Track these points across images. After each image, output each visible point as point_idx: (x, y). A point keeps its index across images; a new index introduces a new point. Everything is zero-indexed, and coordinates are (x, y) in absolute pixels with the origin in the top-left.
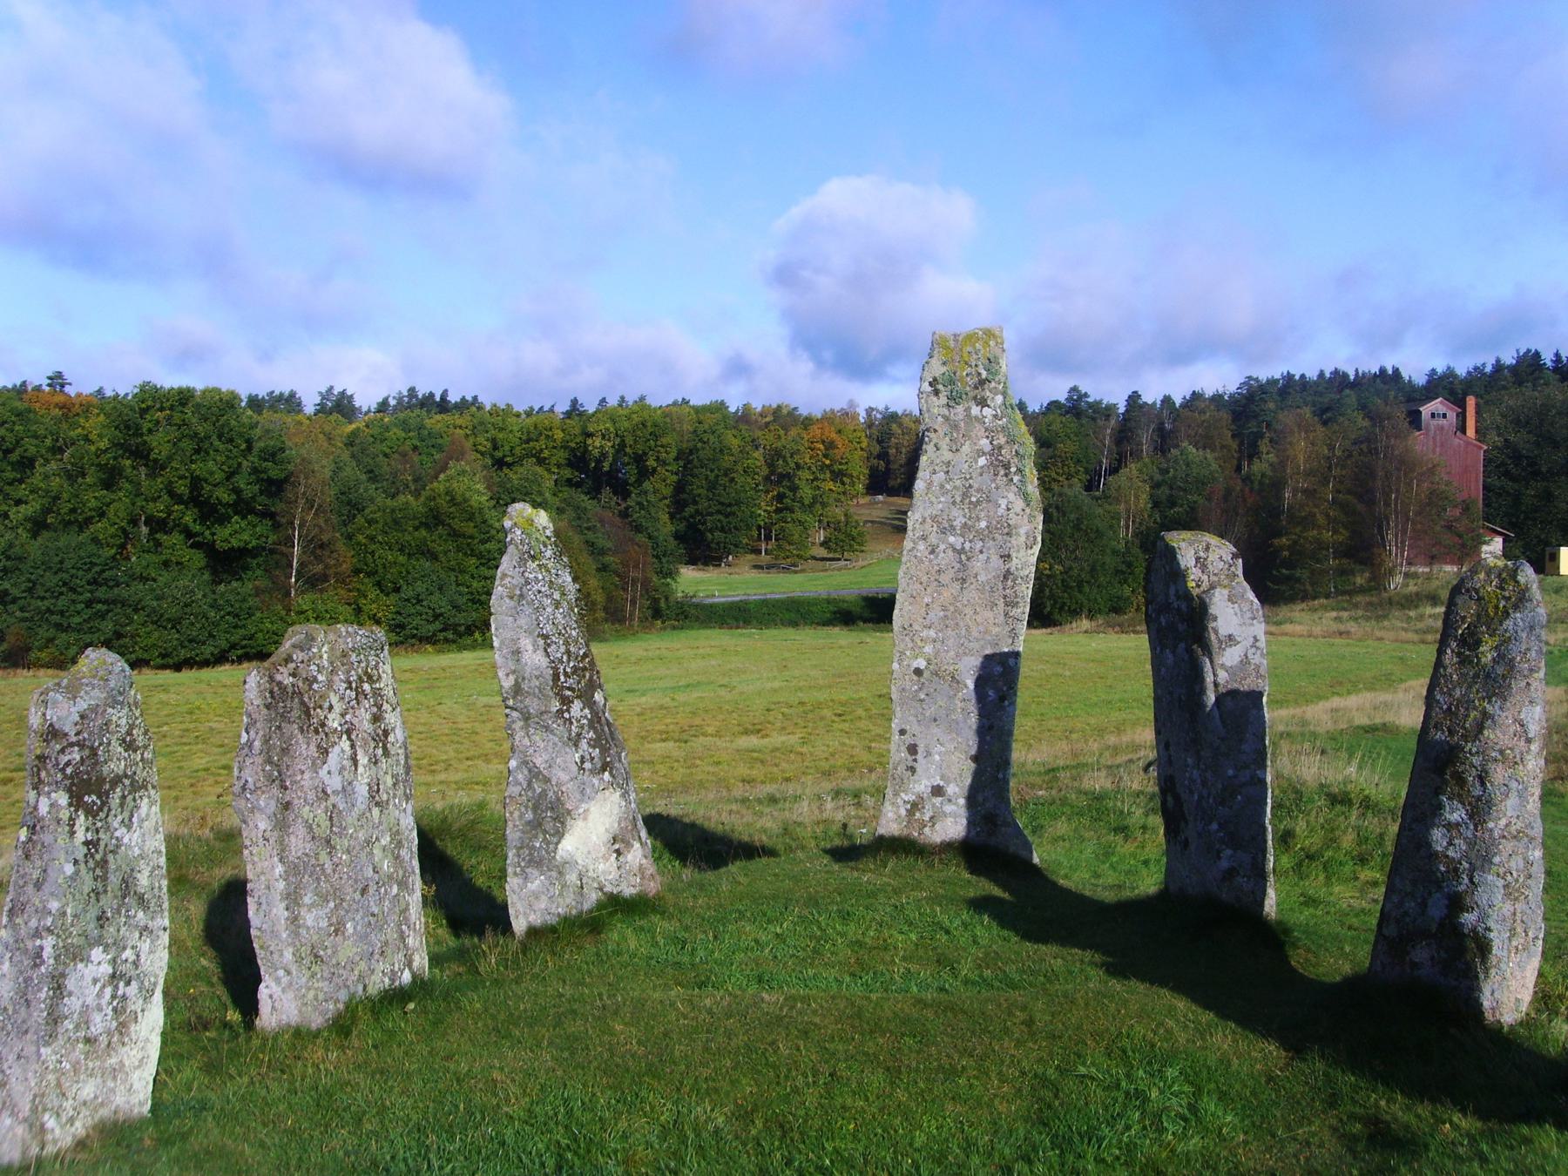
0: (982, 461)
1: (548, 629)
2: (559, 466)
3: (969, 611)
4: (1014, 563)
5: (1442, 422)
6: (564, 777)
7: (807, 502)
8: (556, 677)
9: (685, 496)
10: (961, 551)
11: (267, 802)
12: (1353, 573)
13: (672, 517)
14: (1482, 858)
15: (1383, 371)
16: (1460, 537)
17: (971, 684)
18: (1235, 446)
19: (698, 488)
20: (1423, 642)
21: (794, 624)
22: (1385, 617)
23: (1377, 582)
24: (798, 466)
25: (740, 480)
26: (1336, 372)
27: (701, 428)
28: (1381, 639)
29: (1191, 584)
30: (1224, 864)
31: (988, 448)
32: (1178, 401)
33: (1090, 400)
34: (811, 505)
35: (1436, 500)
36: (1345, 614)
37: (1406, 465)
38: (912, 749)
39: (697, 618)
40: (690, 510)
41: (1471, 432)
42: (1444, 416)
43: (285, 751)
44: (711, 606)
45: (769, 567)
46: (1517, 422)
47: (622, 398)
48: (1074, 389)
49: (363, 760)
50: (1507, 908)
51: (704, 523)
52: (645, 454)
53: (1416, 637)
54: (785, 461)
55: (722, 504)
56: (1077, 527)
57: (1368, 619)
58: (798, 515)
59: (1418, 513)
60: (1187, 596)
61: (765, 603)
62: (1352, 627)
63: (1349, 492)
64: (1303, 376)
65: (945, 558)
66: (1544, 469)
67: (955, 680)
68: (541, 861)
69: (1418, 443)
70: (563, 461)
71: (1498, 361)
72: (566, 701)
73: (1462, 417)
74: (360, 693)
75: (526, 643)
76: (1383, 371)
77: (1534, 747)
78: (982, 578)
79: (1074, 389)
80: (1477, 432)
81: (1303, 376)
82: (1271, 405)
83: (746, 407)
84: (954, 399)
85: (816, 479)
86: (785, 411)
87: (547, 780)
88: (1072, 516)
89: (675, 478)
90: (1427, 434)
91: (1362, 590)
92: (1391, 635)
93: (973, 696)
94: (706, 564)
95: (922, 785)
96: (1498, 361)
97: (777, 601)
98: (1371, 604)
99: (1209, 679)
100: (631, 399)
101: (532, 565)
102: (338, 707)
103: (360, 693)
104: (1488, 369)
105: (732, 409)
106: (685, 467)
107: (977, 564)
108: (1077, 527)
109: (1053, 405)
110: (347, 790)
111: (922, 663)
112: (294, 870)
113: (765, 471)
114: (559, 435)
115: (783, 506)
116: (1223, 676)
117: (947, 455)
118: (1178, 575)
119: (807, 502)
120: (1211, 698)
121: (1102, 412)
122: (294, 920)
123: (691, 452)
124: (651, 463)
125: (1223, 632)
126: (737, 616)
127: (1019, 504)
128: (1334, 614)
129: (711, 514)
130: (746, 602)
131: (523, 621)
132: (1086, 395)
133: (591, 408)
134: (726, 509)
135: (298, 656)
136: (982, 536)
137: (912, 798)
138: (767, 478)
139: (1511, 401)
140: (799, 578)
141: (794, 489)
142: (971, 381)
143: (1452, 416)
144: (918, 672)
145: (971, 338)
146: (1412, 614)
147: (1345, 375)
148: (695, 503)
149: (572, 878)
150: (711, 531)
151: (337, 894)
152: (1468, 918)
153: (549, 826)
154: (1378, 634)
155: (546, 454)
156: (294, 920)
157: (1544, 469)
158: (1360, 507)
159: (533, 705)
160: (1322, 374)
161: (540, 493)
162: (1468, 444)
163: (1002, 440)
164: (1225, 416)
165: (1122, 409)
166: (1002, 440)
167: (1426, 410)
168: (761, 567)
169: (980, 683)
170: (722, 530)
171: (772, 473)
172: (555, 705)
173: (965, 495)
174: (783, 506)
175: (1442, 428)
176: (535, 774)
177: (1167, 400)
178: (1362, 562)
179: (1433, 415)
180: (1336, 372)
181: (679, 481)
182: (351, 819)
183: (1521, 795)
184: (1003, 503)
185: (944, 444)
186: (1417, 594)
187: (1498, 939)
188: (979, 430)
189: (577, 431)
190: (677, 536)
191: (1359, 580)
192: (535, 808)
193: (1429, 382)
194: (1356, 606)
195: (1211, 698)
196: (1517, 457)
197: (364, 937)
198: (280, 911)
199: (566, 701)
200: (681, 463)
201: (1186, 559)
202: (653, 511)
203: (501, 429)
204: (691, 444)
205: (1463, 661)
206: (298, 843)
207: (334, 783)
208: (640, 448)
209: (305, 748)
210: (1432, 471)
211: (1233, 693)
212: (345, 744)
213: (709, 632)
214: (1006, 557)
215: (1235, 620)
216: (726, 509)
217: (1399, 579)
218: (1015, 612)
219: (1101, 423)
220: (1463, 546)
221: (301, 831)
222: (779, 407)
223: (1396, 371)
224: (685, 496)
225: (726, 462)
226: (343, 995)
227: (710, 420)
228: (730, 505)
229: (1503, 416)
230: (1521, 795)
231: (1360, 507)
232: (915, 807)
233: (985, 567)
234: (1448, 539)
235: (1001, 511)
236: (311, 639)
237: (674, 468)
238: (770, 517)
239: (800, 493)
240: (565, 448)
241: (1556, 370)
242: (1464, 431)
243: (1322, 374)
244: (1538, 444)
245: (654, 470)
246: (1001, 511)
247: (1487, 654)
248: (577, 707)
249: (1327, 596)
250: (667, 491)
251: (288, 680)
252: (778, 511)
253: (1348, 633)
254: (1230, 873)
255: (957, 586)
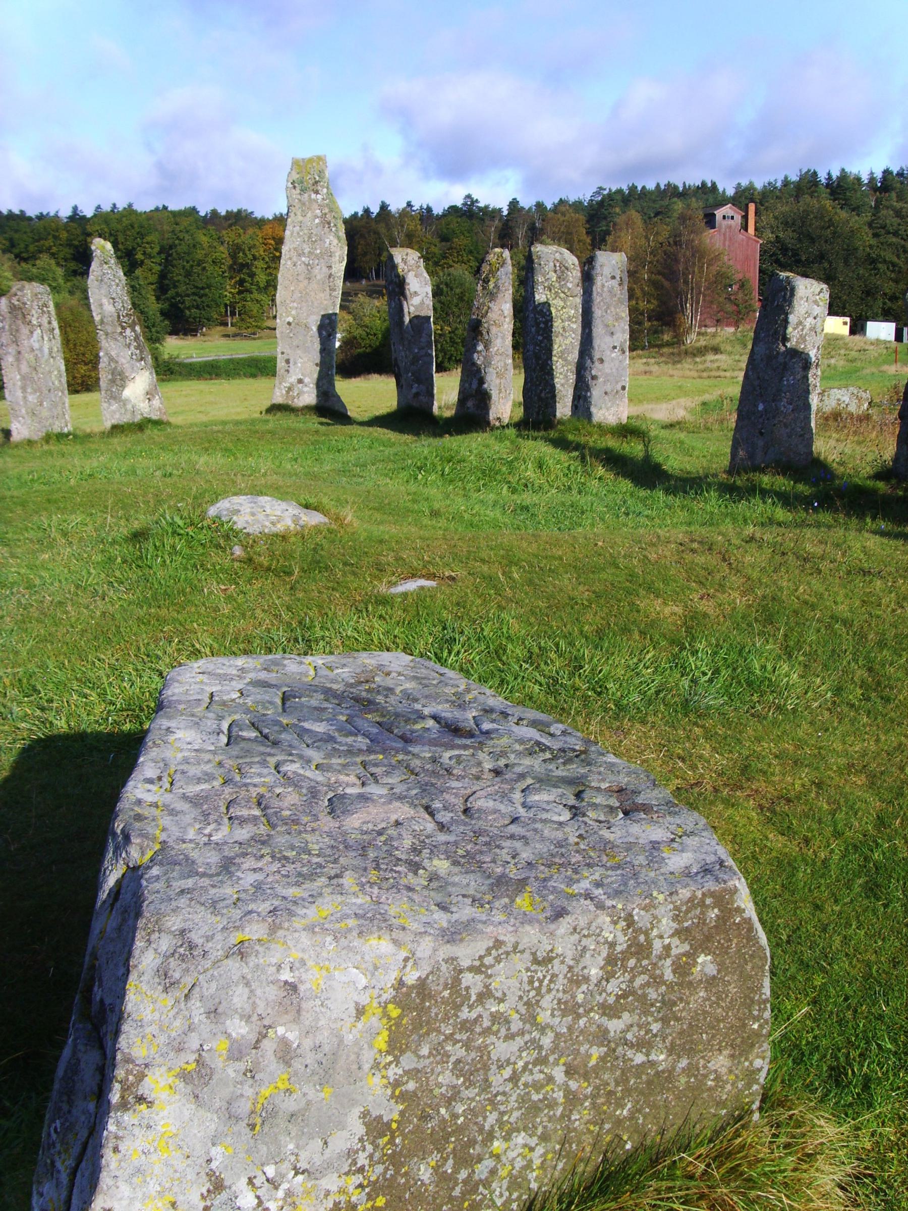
0: (317, 221)
1: (114, 295)
2: (66, 260)
3: (312, 294)
4: (334, 270)
5: (730, 222)
6: (124, 361)
7: (262, 285)
8: (119, 317)
9: (167, 282)
10: (308, 265)
11: (12, 350)
12: (662, 332)
13: (158, 299)
14: (488, 363)
15: (704, 184)
16: (738, 306)
17: (315, 329)
18: (588, 240)
19: (177, 274)
20: (700, 377)
21: (254, 376)
22: (679, 362)
23: (678, 340)
24: (255, 258)
25: (210, 268)
26: (669, 185)
27: (178, 228)
28: (671, 376)
29: (400, 270)
30: (414, 391)
31: (320, 214)
32: (549, 206)
33: (481, 205)
34: (266, 288)
35: (722, 280)
36: (653, 360)
37: (699, 253)
38: (288, 361)
39: (180, 374)
40: (171, 293)
41: (751, 230)
42: (732, 218)
43: (17, 331)
44: (191, 364)
45: (235, 335)
46: (786, 224)
47: (114, 205)
48: (468, 196)
49: (46, 338)
50: (498, 381)
51: (183, 303)
52: (134, 249)
53: (695, 374)
54: (244, 254)
55: (197, 287)
56: (461, 299)
57: (666, 363)
58: (256, 295)
59: (708, 288)
60: (398, 276)
61: (231, 361)
62: (655, 368)
63: (659, 273)
64: (644, 188)
65: (300, 268)
66: (804, 259)
67: (307, 327)
68: (115, 397)
69: (712, 239)
70: (69, 256)
71: (786, 178)
72: (123, 328)
73: (745, 218)
74: (43, 312)
75: (105, 301)
76: (704, 184)
77: (507, 320)
78: (318, 277)
79: (468, 196)
80: (756, 230)
81: (644, 188)
82: (617, 210)
83: (214, 213)
84: (303, 191)
85: (269, 267)
86: (243, 214)
87: (117, 362)
88: (458, 291)
89: (158, 268)
90: (719, 231)
91: (668, 344)
92: (681, 373)
93: (317, 334)
94: (185, 334)
95: (293, 379)
96: (786, 178)
97: (241, 359)
98: (673, 354)
99: (406, 310)
100: (121, 206)
101: (106, 266)
102: (36, 316)
103: (43, 312)
104: (779, 184)
105: (202, 214)
106: (166, 259)
107: (316, 271)
108: (461, 299)
109: (453, 209)
110: (41, 349)
111: (290, 319)
112: (24, 378)
113: (229, 262)
114: (64, 235)
115: (243, 288)
116: (412, 309)
117: (300, 218)
118: (394, 267)
119: (262, 285)
120: (407, 319)
121: (489, 214)
122: (25, 398)
123: (171, 247)
124: (139, 256)
125: (412, 290)
126: (210, 371)
127: (335, 241)
128: (645, 360)
129: (188, 296)
130: (217, 361)
131: (103, 291)
132: (477, 201)
133: (89, 213)
134: (199, 292)
135: (19, 293)
136: (318, 257)
137: (288, 385)
138: (231, 267)
139: (783, 208)
140: (258, 343)
141: (252, 275)
142: (311, 182)
143: (738, 219)
144: (289, 324)
145: (311, 160)
146: (698, 360)
147: (676, 187)
148: (175, 287)
149: (129, 407)
150: (189, 308)
151: (39, 390)
152: (485, 386)
153: (118, 382)
154: (671, 372)
155: (54, 249)
156: (25, 398)
157: (804, 259)
158: (666, 284)
159: (109, 329)
160: (658, 185)
161: (54, 279)
162: (749, 238)
163: (327, 210)
164: (582, 218)
165: (505, 213)
166: (327, 210)
167: (719, 213)
168: (228, 336)
169: (320, 328)
170: (197, 307)
171: (235, 263)
172: (119, 330)
173: (310, 237)
174: (243, 288)
175: (730, 227)
176: (111, 359)
177: (539, 205)
178: (668, 324)
179: (724, 217)
180: (669, 185)
181: (162, 271)
182: (43, 361)
183: (503, 338)
184: (328, 241)
185: (299, 213)
186: (705, 347)
187: (494, 394)
188: (315, 206)
189: (79, 231)
190: (163, 313)
191: (666, 337)
192: (113, 374)
193: (736, 193)
194: (662, 355)
195: (407, 319)
196: (784, 249)
197: (50, 410)
198: (19, 394)
199: (123, 328)
200: (163, 256)
201: (398, 259)
202: (143, 292)
203: (16, 231)
204: (170, 242)
205: (484, 288)
206: (25, 368)
207: (36, 346)
208: (129, 245)
209: (25, 330)
210: (717, 257)
211: (417, 317)
212: (39, 331)
213: (189, 383)
214: (330, 267)
215: (418, 285)
216: (199, 292)
217: (693, 336)
218: (334, 293)
219: (487, 222)
220: (739, 312)
221: (25, 363)
222: (239, 211)
223: (714, 185)
224: (167, 282)
225: (199, 254)
226: (44, 430)
227: (185, 222)
228: (203, 288)
229: (776, 218)
230: (503, 338)
231: (666, 284)
232: (290, 389)
233: (320, 272)
234: (729, 308)
235: (327, 245)
236: (24, 287)
237: (158, 260)
238: (234, 297)
239: (257, 278)
240: (70, 245)
241: (828, 186)
242: (746, 230)
243: (658, 185)
244: (800, 240)
245: (142, 262)
246: (327, 245)
247: (491, 285)
248: (128, 331)
249: (643, 349)
250: (153, 278)
251: (16, 303)
252: (240, 293)
253: (651, 372)
254: (417, 395)
255: (306, 281)
